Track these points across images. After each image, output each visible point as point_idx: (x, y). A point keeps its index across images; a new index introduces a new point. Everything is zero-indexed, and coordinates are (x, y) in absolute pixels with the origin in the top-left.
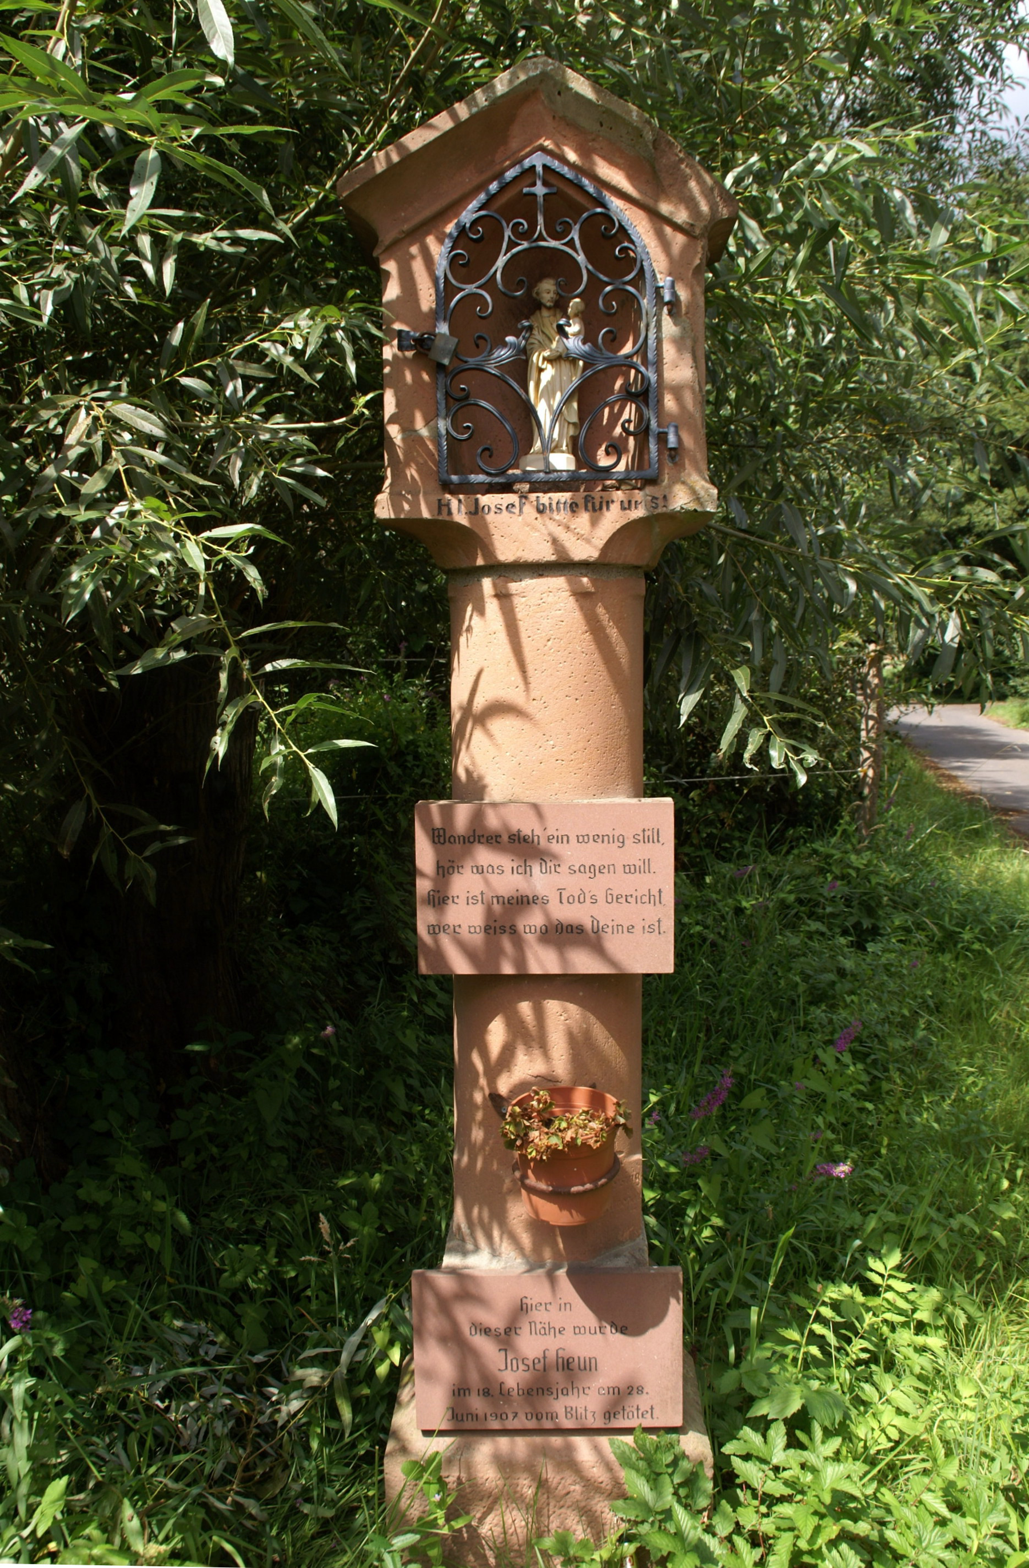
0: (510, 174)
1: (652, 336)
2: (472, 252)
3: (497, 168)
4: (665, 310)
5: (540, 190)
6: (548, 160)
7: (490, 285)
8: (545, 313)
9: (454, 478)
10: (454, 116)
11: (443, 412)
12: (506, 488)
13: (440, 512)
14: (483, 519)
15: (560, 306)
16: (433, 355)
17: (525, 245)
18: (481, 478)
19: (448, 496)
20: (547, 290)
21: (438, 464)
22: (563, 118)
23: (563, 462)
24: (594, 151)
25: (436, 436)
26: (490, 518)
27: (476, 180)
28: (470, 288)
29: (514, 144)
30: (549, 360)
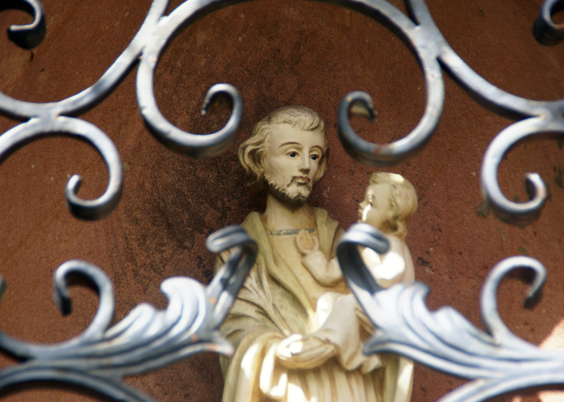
8: (279, 218)
15: (330, 197)
20: (290, 144)
28: (48, 116)
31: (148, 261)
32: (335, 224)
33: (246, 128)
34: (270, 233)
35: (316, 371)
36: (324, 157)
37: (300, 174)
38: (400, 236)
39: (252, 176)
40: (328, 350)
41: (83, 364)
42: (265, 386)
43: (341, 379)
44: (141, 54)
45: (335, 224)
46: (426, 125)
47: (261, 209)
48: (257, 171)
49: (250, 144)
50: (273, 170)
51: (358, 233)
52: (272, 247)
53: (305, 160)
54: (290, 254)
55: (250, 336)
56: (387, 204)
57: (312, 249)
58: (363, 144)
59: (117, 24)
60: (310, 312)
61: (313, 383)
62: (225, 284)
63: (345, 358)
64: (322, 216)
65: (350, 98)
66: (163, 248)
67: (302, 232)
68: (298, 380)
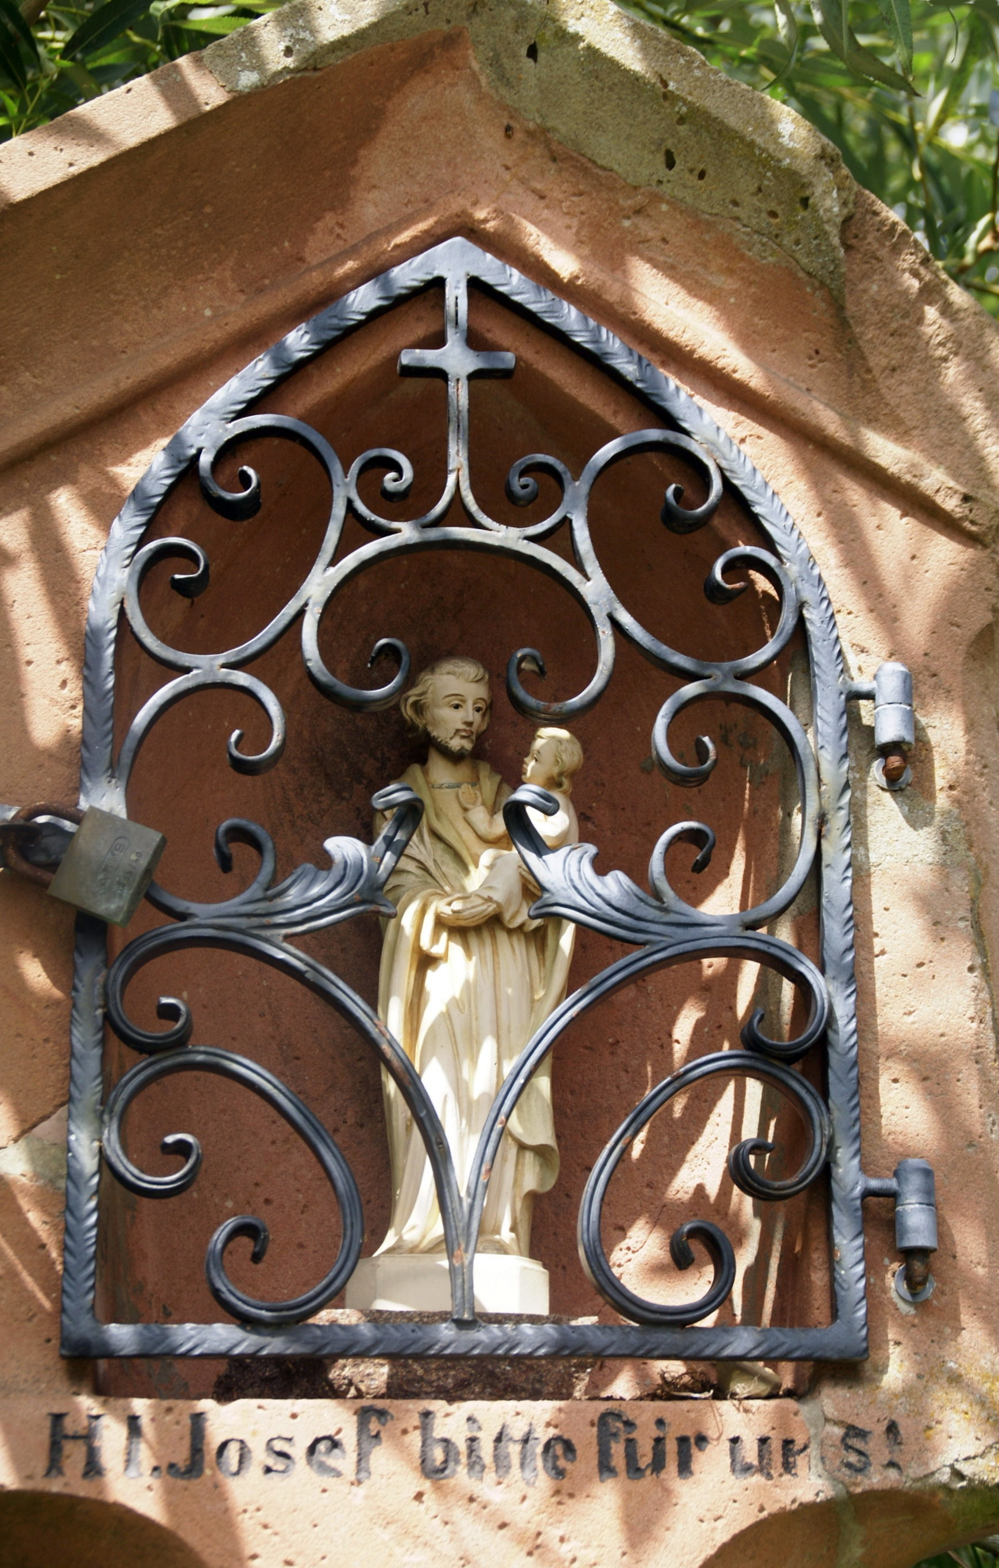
0: (364, 299)
1: (836, 857)
2: (218, 544)
3: (314, 281)
4: (876, 772)
5: (456, 359)
6: (490, 268)
7: (279, 659)
8: (440, 771)
9: (122, 1335)
10: (176, 92)
11: (90, 1091)
12: (301, 1376)
13: (54, 1465)
14: (218, 1491)
15: (495, 753)
16: (66, 886)
17: (407, 533)
18: (222, 1336)
19: (87, 1403)
20: (454, 696)
21: (58, 1288)
22: (540, 135)
23: (510, 1284)
24: (639, 246)
25: (59, 1181)
26: (245, 1490)
27: (241, 314)
28: (208, 666)
29: (369, 208)
30: (460, 930)
31: (305, 812)
32: (498, 778)
33: (410, 682)
34: (431, 786)
35: (478, 929)
36: (489, 709)
37: (463, 727)
38: (564, 793)
39: (413, 727)
40: (491, 908)
41: (243, 923)
42: (425, 943)
43: (502, 937)
44: (306, 604)
45: (498, 778)
46: (597, 682)
47: (423, 760)
48: (418, 721)
49: (413, 694)
50: (435, 722)
51: (522, 795)
52: (434, 801)
53: (468, 713)
54: (453, 810)
55: (411, 893)
56: (553, 759)
57: (474, 803)
58: (532, 701)
59: (278, 569)
60: (472, 868)
61: (473, 941)
62: (389, 842)
63: (507, 916)
64: (485, 770)
65: (519, 655)
66: (321, 799)
67: (465, 787)
68: (458, 938)
